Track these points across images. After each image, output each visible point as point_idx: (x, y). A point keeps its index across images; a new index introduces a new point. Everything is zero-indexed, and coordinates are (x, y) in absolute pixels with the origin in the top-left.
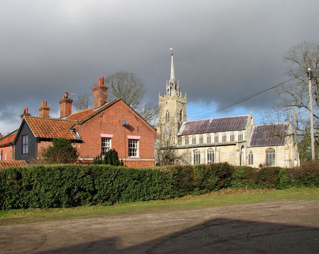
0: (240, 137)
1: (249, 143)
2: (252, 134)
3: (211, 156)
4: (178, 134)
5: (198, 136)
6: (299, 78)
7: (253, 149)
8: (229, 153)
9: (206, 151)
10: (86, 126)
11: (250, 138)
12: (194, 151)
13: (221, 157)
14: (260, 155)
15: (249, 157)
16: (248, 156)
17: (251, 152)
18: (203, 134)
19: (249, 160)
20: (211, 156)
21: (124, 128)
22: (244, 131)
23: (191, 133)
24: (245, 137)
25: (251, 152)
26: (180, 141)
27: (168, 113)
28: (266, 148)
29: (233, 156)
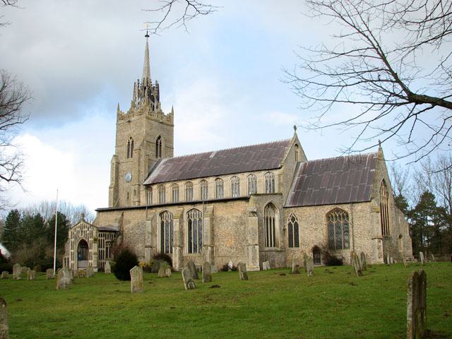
0: (270, 184)
1: (289, 199)
2: (297, 178)
3: (95, 268)
4: (146, 183)
5: (182, 185)
6: (389, 94)
7: (298, 212)
8: (235, 221)
9: (185, 216)
10: (254, 165)
11: (293, 188)
12: (161, 214)
13: (216, 229)
14: (314, 226)
15: (290, 230)
16: (287, 227)
17: (293, 219)
18: (239, 176)
19: (290, 236)
20: (95, 268)
21: (158, 136)
22: (276, 172)
23: (175, 180)
24: (280, 184)
25: (293, 219)
26: (148, 196)
27: (131, 141)
28: (328, 209)
29: (242, 228)
